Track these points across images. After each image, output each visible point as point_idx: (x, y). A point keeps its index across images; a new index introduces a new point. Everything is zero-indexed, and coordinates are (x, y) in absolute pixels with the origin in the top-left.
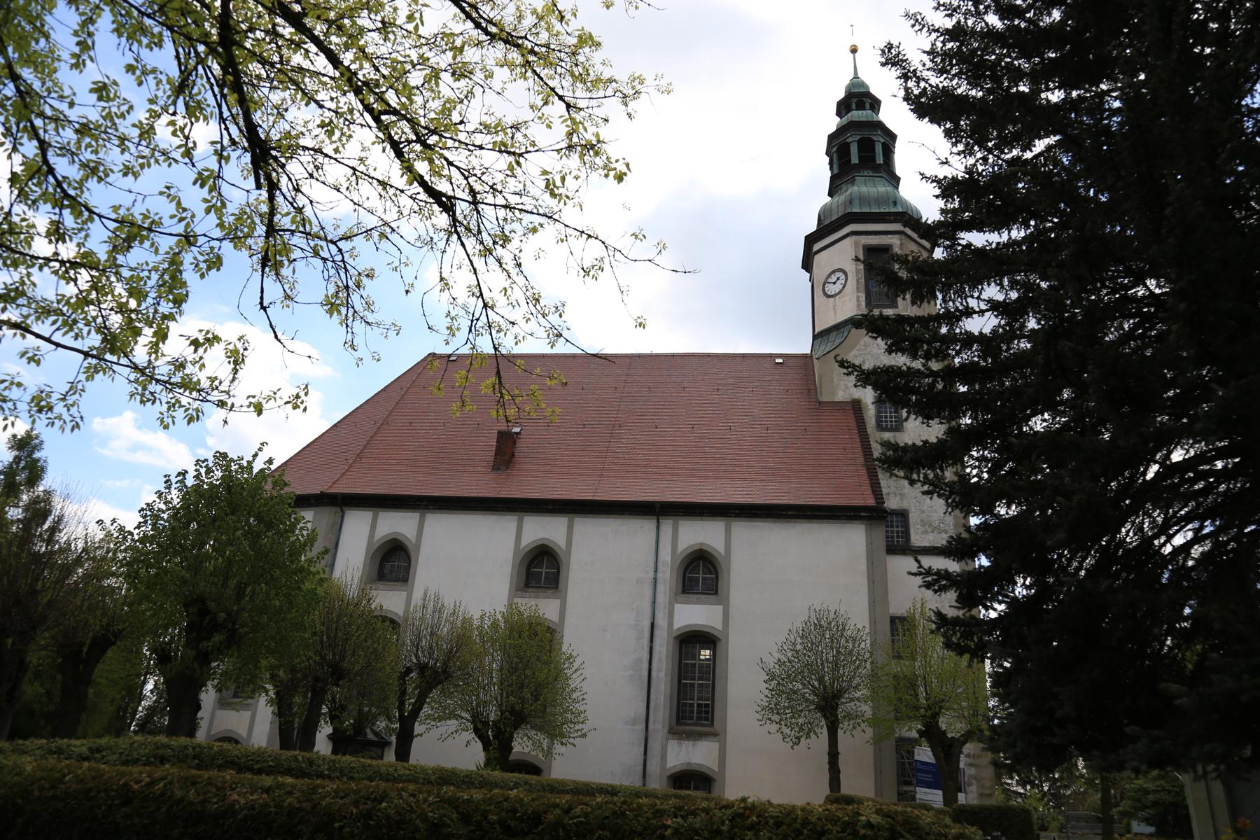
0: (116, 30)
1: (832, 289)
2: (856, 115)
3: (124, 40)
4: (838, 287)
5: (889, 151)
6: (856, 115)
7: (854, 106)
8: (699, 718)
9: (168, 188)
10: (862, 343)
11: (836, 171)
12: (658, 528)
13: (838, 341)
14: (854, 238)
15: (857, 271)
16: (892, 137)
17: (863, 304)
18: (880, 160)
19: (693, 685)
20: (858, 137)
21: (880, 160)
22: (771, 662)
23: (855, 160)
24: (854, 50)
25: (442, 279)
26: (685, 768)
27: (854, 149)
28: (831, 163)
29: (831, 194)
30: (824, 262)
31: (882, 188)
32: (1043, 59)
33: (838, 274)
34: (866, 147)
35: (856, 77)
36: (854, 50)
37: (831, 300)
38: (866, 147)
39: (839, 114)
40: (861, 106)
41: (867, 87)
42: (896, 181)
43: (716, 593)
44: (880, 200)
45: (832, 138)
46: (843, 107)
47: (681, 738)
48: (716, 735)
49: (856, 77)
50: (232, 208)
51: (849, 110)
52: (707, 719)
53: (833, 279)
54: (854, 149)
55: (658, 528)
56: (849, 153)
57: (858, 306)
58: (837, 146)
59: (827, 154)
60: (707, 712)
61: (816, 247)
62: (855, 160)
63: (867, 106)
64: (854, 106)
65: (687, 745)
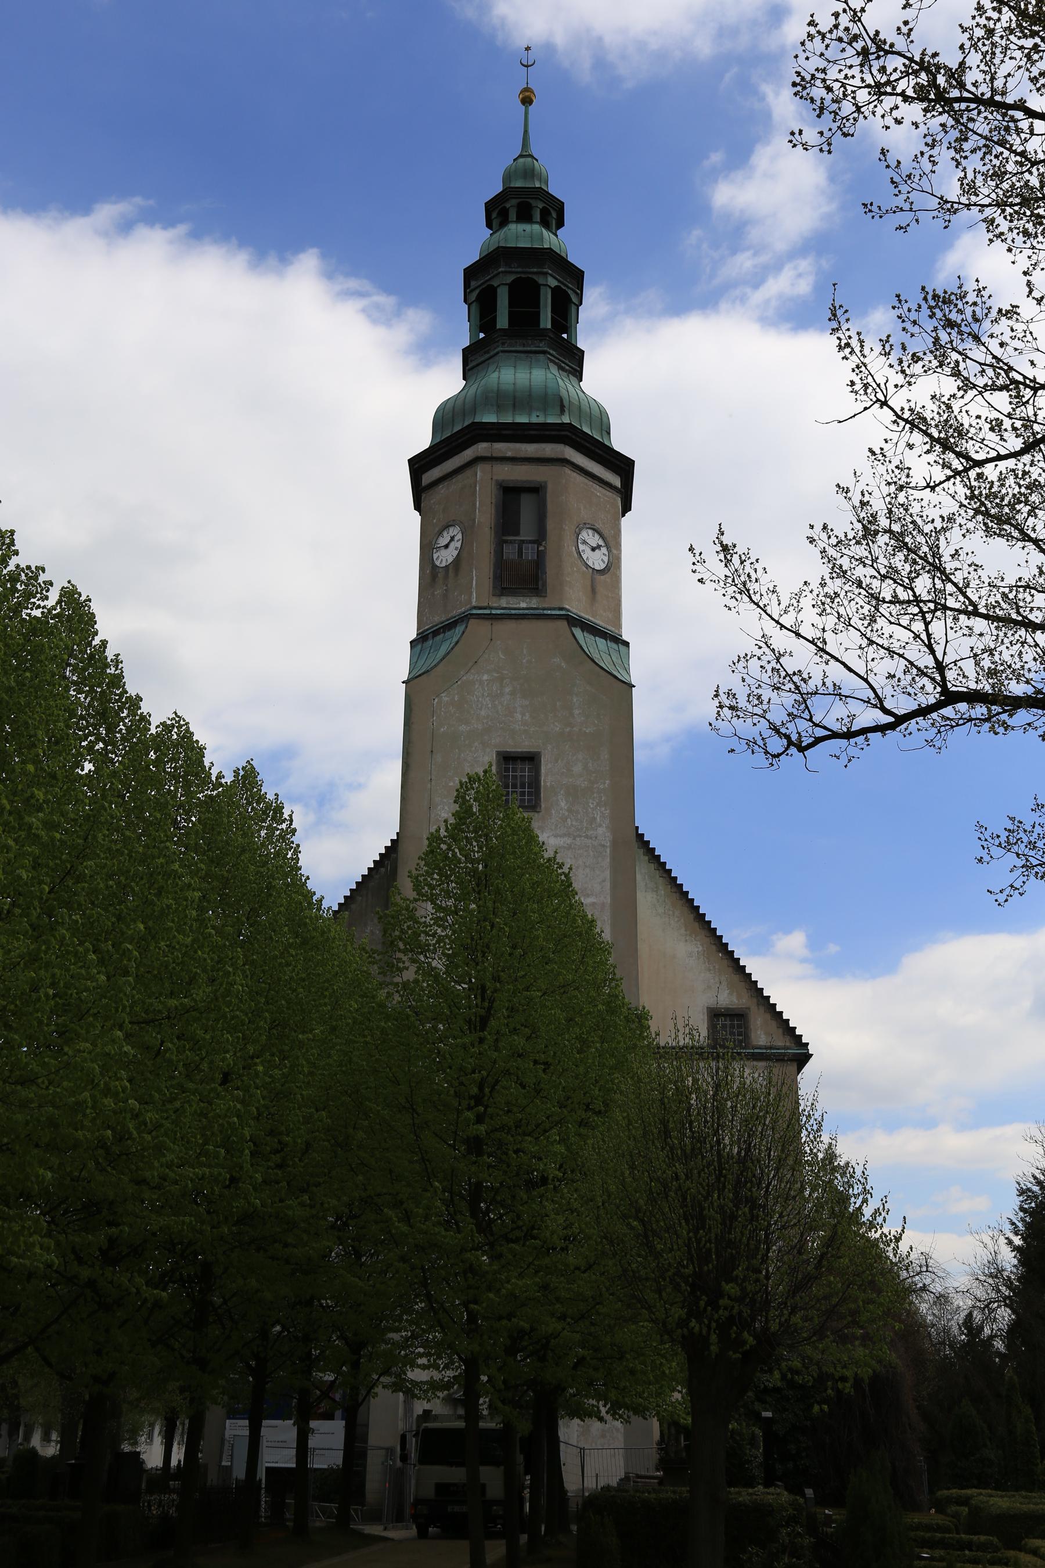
2: (521, 234)
3: (826, 1138)
6: (521, 234)
7: (513, 215)
9: (980, 860)
13: (444, 649)
18: (546, 321)
20: (510, 279)
21: (546, 321)
23: (503, 321)
25: (717, 691)
29: (464, 379)
34: (525, 295)
35: (525, 154)
38: (525, 295)
40: (524, 216)
46: (497, 212)
49: (525, 154)
62: (503, 321)
63: (537, 216)
64: (513, 215)
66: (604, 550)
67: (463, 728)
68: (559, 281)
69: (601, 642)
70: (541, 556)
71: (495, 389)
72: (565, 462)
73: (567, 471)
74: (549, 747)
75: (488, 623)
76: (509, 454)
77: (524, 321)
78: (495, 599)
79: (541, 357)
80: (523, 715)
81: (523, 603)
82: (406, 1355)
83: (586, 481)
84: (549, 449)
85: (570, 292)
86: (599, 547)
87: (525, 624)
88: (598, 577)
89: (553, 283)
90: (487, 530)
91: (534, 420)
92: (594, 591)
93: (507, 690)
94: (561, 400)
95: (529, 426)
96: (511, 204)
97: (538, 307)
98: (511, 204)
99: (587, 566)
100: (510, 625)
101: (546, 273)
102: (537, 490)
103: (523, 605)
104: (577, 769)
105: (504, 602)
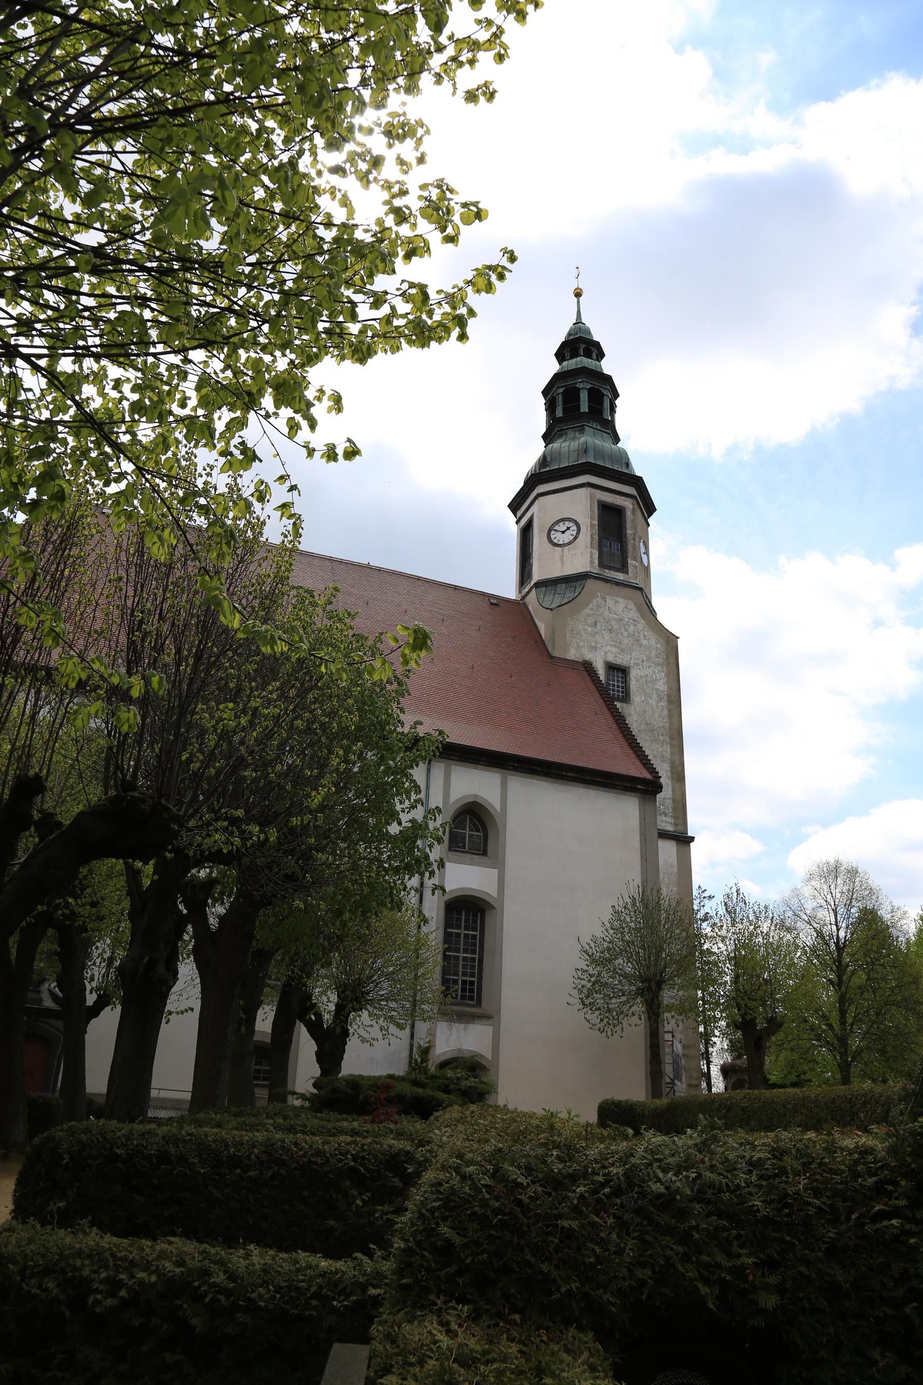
1: (558, 538)
4: (567, 537)
8: (463, 997)
10: (594, 602)
11: (559, 413)
12: (429, 770)
13: (572, 595)
14: (589, 490)
15: (592, 526)
17: (596, 561)
19: (457, 958)
20: (589, 386)
22: (586, 939)
23: (584, 407)
24: (578, 294)
26: (455, 1055)
27: (584, 396)
30: (545, 510)
31: (604, 443)
33: (568, 524)
35: (579, 321)
36: (578, 294)
37: (557, 549)
39: (560, 355)
40: (588, 354)
41: (589, 333)
43: (485, 853)
47: (451, 1020)
48: (489, 1017)
49: (579, 321)
50: (149, 293)
52: (471, 998)
53: (562, 527)
54: (584, 396)
55: (429, 770)
56: (578, 399)
57: (592, 562)
60: (472, 991)
62: (584, 407)
65: (458, 1027)
86: (568, 528)
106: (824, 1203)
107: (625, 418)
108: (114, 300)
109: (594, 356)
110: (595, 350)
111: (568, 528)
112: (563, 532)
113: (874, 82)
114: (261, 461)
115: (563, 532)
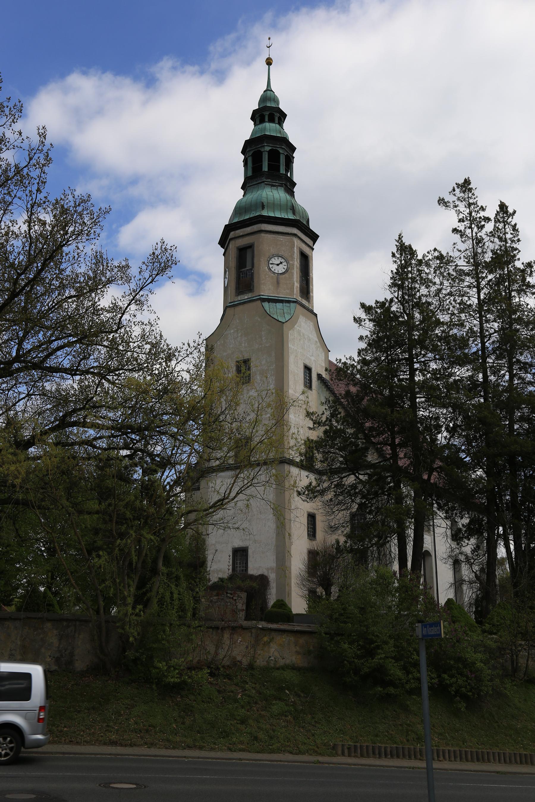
0: (308, 440)
2: (270, 128)
5: (289, 161)
6: (270, 128)
7: (267, 119)
11: (250, 174)
16: (293, 149)
23: (265, 168)
24: (269, 62)
27: (265, 157)
28: (245, 162)
31: (278, 194)
32: (508, 495)
34: (274, 156)
35: (269, 89)
38: (274, 156)
42: (289, 186)
44: (280, 207)
45: (247, 143)
46: (258, 116)
49: (269, 89)
51: (262, 121)
54: (265, 157)
56: (261, 161)
58: (252, 149)
59: (243, 152)
61: (232, 234)
62: (265, 168)
64: (267, 119)
66: (285, 263)
67: (225, 354)
68: (271, 146)
69: (279, 305)
70: (252, 275)
71: (279, 203)
72: (261, 231)
73: (263, 235)
74: (254, 355)
75: (233, 308)
76: (241, 234)
77: (274, 166)
78: (236, 297)
79: (263, 184)
80: (245, 344)
81: (246, 297)
82: (260, 675)
83: (274, 236)
84: (255, 228)
85: (278, 149)
86: (281, 263)
87: (246, 306)
88: (281, 276)
89: (268, 149)
90: (233, 269)
91: (252, 216)
92: (278, 283)
93: (239, 335)
94: (263, 203)
95: (250, 219)
96: (267, 114)
97: (262, 162)
98: (267, 114)
99: (274, 273)
100: (241, 307)
101: (264, 146)
102: (251, 247)
103: (246, 297)
104: (264, 362)
105: (239, 298)
106: (146, 555)
107: (300, 171)
108: (410, 532)
109: (277, 121)
110: (280, 117)
111: (281, 263)
112: (278, 265)
113: (268, 16)
114: (400, 237)
115: (278, 265)
